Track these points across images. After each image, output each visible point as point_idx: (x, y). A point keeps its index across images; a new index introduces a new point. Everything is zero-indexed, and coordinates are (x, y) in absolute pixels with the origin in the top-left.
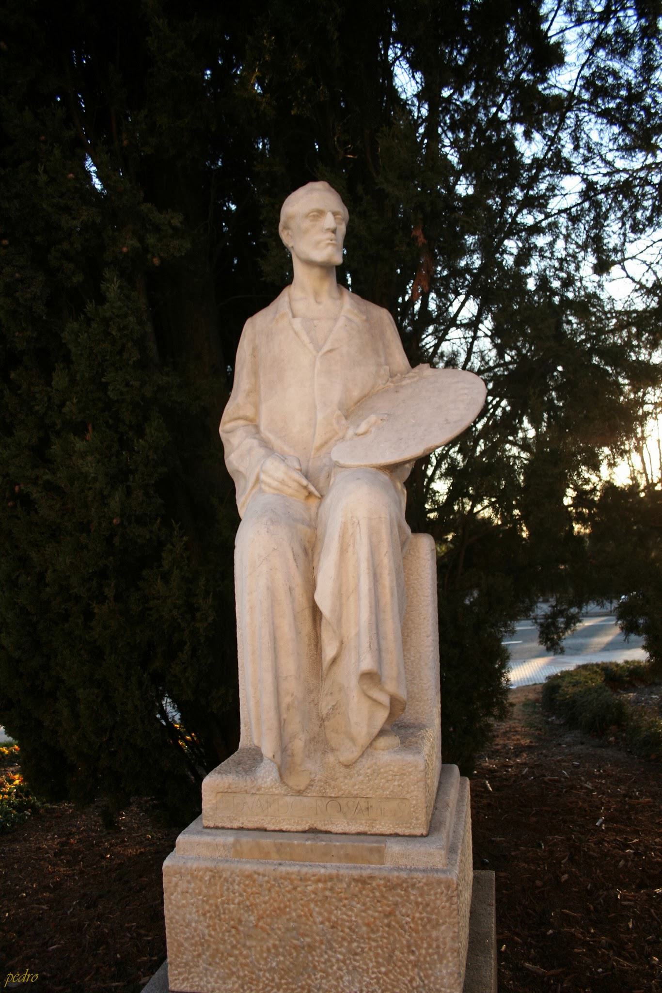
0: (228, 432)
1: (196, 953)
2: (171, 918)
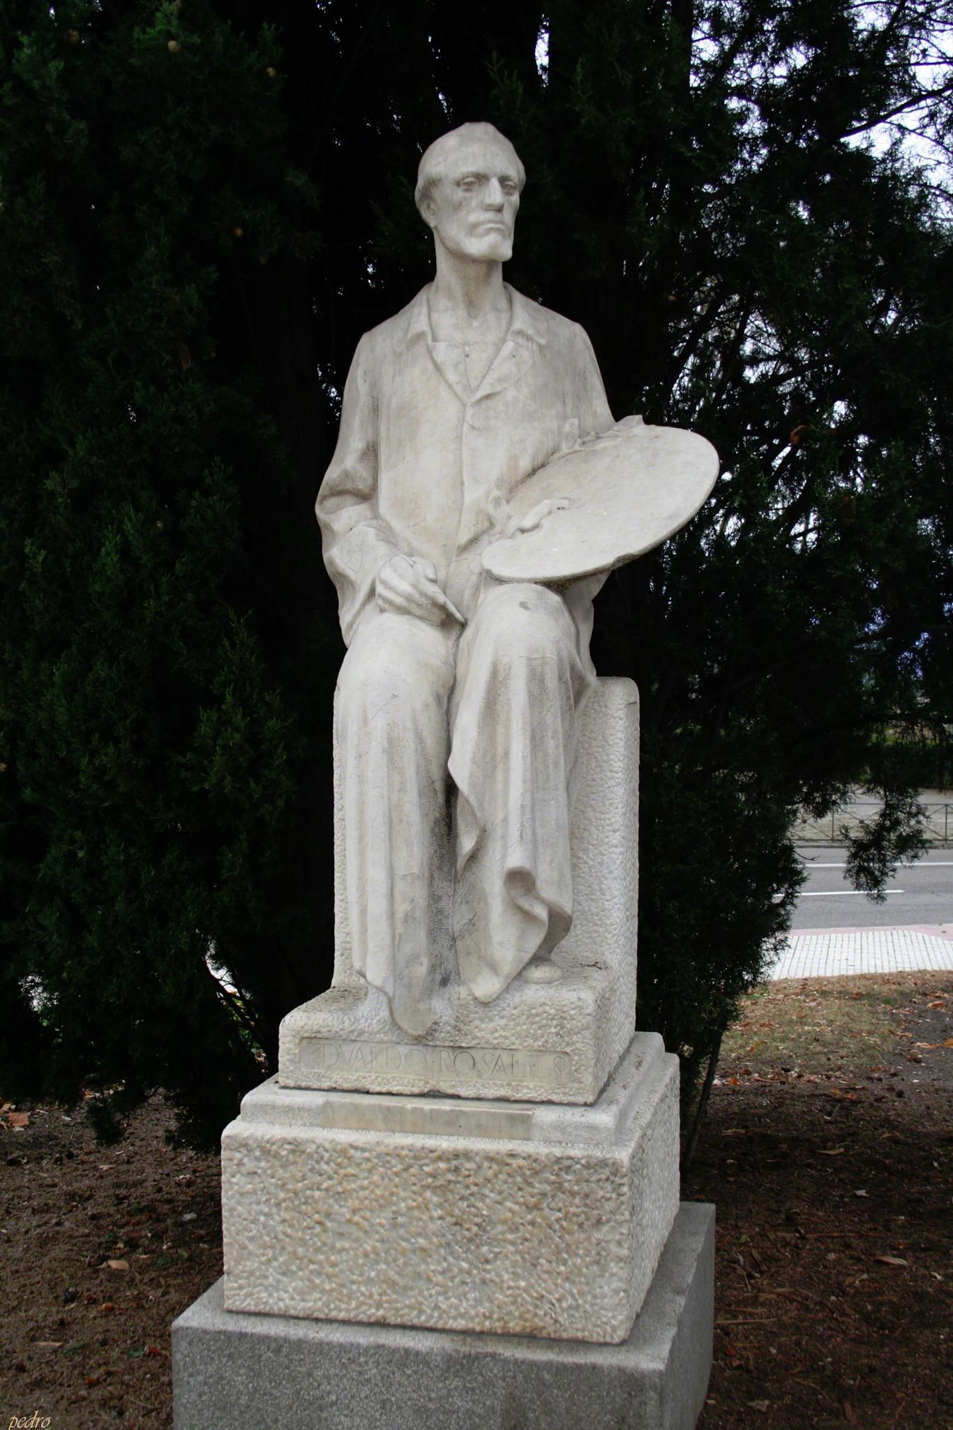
1: (263, 1259)
2: (232, 1210)
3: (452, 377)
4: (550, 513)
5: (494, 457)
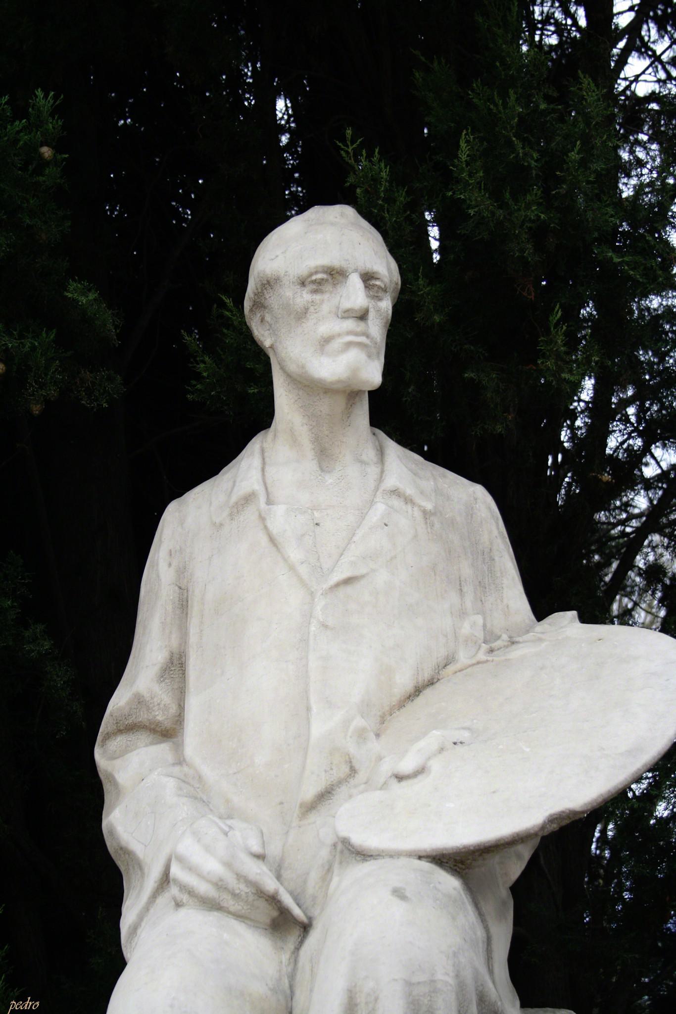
0: (113, 758)
3: (295, 554)
4: (441, 750)
5: (359, 667)
